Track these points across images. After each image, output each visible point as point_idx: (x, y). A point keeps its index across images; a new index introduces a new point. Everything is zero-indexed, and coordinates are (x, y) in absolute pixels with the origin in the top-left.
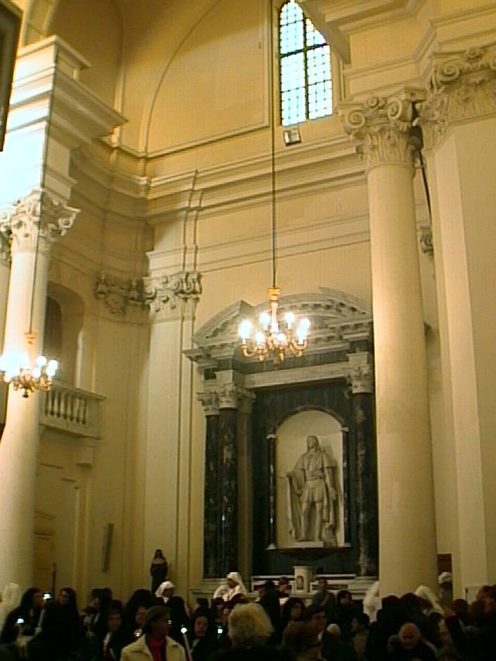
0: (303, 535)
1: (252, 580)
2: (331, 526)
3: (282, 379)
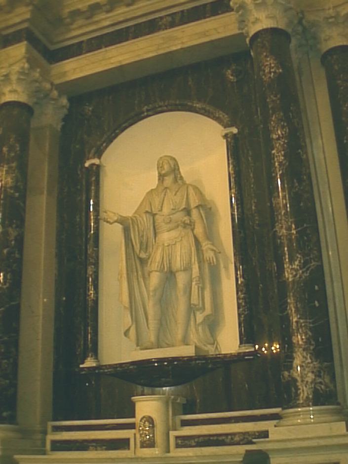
0: (151, 336)
1: (49, 429)
2: (207, 317)
3: (112, 61)
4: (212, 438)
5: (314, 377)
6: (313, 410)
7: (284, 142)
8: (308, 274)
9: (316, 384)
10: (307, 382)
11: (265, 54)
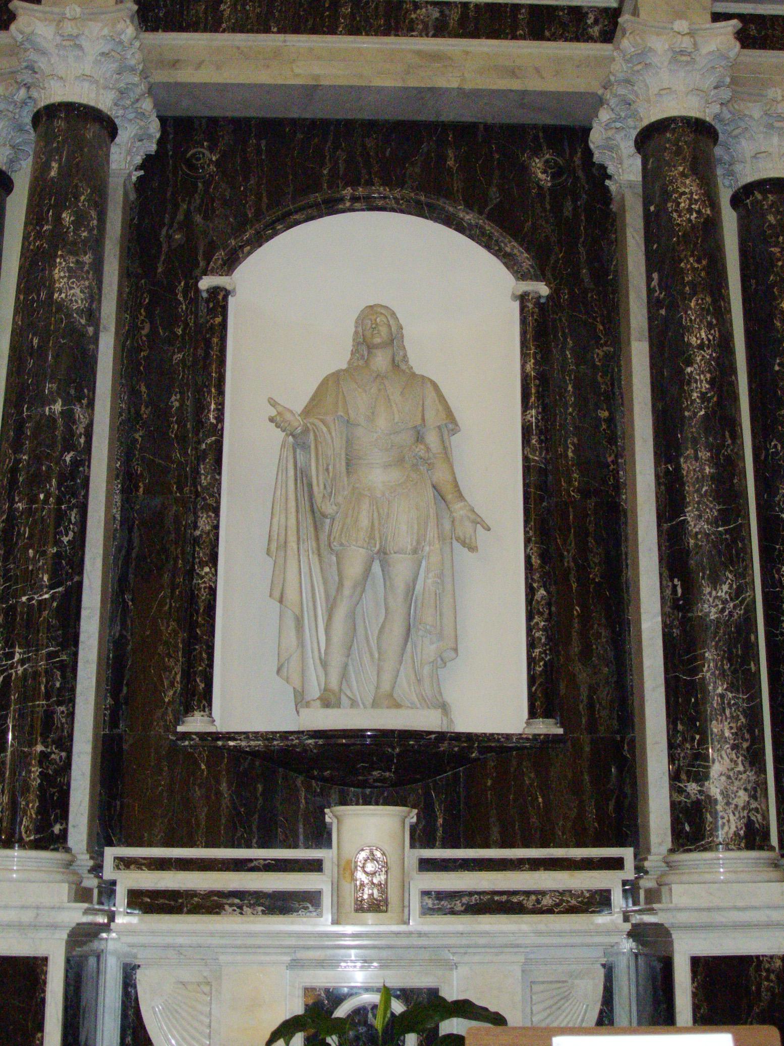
4: (496, 898)
5: (747, 799)
6: (18, 857)
7: (711, 355)
8: (742, 612)
9: (750, 811)
10: (736, 806)
11: (681, 169)
